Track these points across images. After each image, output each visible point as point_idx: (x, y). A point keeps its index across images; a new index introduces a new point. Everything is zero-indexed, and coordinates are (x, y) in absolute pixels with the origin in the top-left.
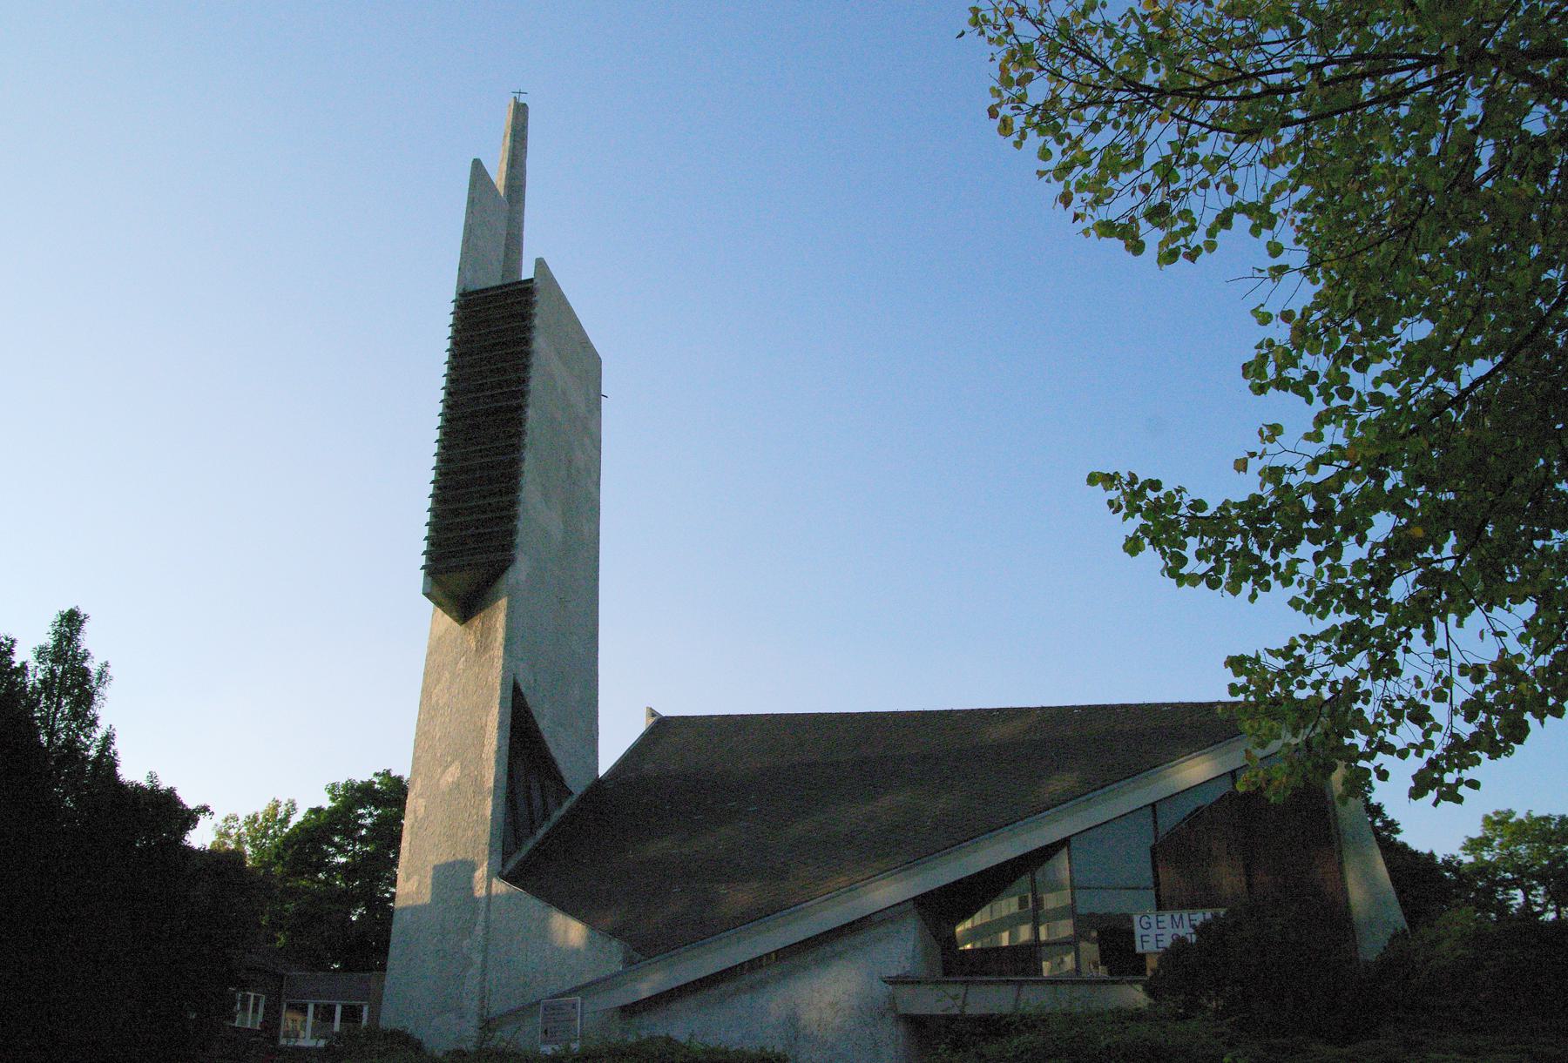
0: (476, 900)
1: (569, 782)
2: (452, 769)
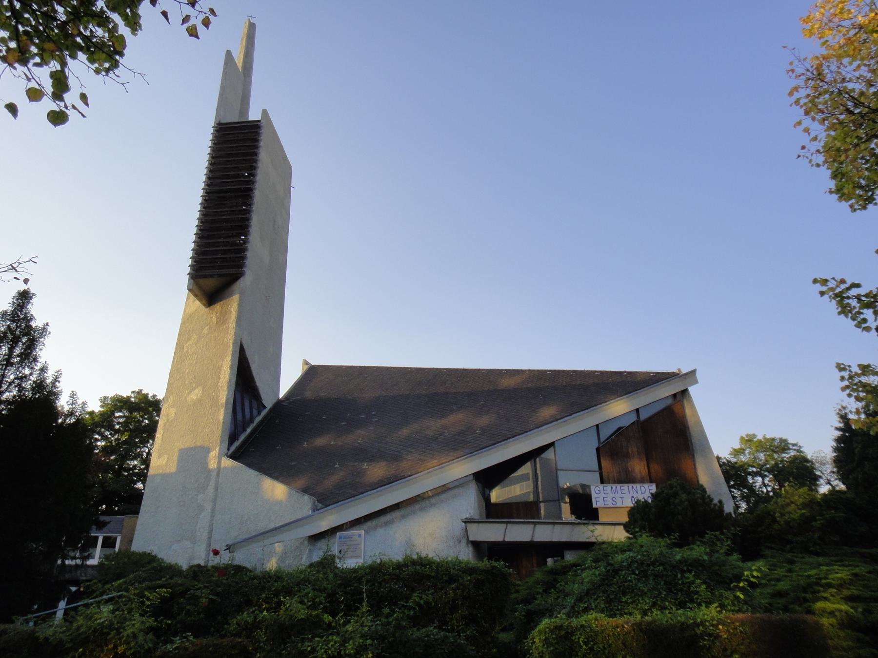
0: (210, 471)
1: (264, 402)
2: (196, 391)
